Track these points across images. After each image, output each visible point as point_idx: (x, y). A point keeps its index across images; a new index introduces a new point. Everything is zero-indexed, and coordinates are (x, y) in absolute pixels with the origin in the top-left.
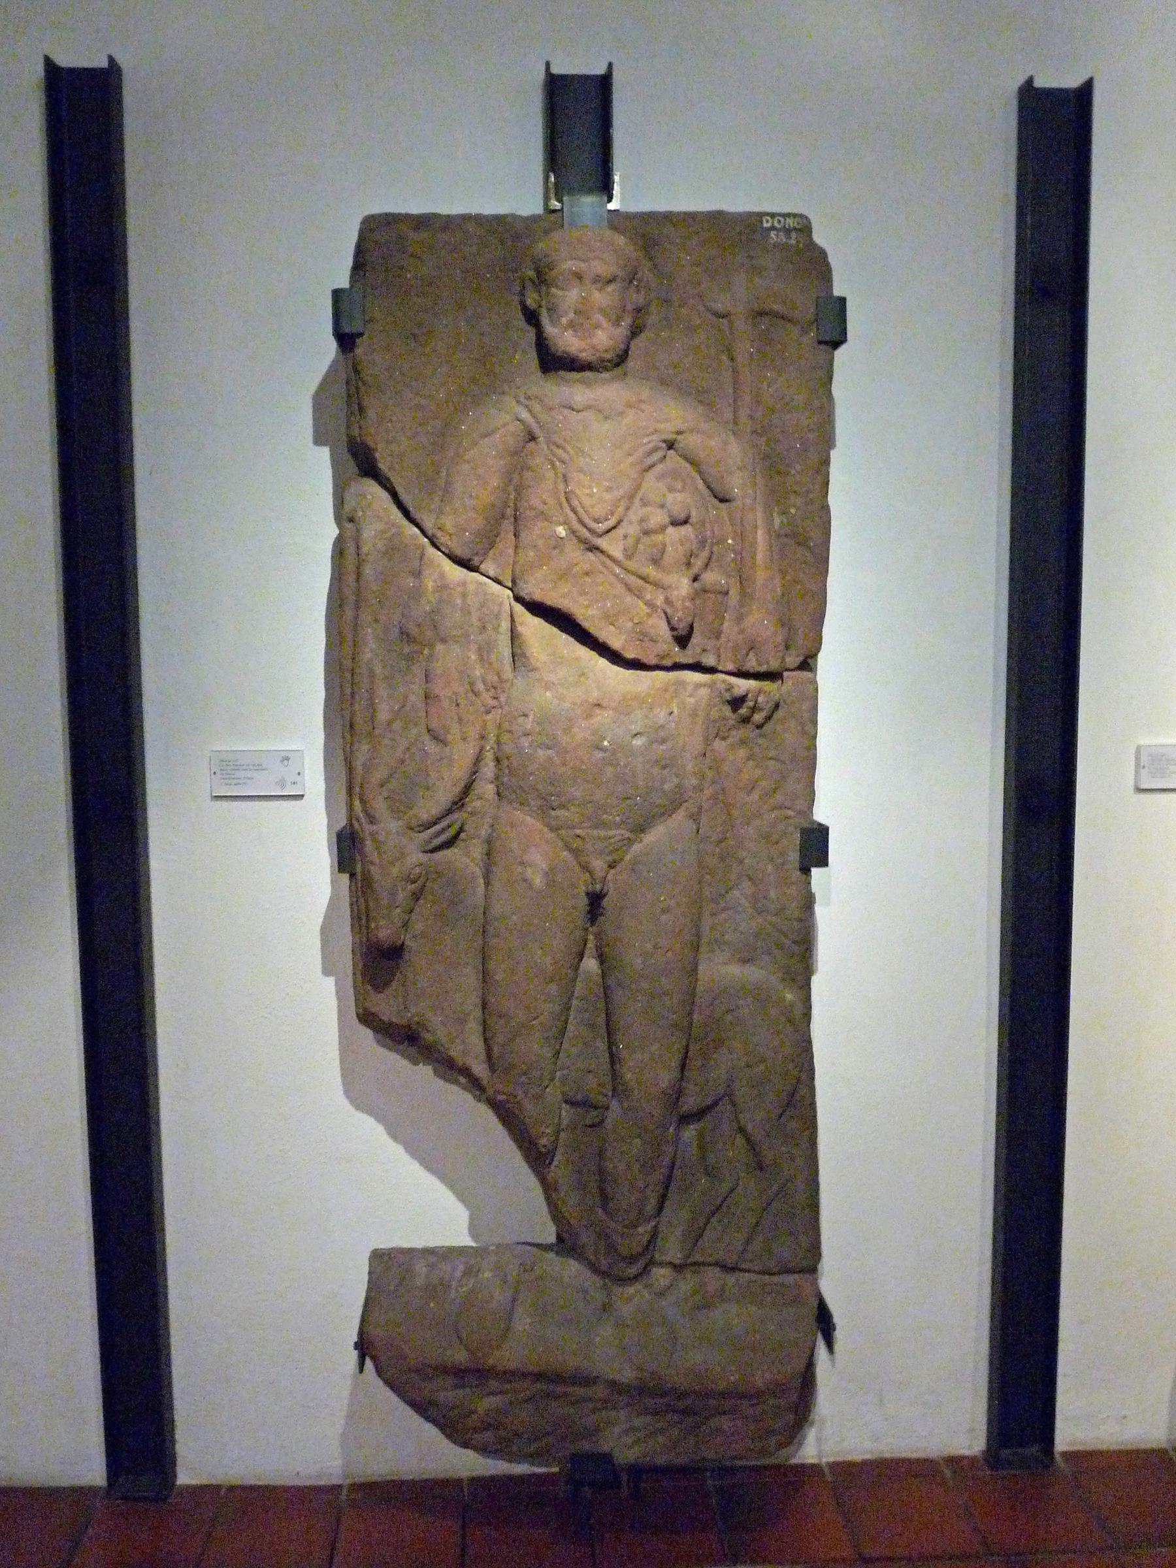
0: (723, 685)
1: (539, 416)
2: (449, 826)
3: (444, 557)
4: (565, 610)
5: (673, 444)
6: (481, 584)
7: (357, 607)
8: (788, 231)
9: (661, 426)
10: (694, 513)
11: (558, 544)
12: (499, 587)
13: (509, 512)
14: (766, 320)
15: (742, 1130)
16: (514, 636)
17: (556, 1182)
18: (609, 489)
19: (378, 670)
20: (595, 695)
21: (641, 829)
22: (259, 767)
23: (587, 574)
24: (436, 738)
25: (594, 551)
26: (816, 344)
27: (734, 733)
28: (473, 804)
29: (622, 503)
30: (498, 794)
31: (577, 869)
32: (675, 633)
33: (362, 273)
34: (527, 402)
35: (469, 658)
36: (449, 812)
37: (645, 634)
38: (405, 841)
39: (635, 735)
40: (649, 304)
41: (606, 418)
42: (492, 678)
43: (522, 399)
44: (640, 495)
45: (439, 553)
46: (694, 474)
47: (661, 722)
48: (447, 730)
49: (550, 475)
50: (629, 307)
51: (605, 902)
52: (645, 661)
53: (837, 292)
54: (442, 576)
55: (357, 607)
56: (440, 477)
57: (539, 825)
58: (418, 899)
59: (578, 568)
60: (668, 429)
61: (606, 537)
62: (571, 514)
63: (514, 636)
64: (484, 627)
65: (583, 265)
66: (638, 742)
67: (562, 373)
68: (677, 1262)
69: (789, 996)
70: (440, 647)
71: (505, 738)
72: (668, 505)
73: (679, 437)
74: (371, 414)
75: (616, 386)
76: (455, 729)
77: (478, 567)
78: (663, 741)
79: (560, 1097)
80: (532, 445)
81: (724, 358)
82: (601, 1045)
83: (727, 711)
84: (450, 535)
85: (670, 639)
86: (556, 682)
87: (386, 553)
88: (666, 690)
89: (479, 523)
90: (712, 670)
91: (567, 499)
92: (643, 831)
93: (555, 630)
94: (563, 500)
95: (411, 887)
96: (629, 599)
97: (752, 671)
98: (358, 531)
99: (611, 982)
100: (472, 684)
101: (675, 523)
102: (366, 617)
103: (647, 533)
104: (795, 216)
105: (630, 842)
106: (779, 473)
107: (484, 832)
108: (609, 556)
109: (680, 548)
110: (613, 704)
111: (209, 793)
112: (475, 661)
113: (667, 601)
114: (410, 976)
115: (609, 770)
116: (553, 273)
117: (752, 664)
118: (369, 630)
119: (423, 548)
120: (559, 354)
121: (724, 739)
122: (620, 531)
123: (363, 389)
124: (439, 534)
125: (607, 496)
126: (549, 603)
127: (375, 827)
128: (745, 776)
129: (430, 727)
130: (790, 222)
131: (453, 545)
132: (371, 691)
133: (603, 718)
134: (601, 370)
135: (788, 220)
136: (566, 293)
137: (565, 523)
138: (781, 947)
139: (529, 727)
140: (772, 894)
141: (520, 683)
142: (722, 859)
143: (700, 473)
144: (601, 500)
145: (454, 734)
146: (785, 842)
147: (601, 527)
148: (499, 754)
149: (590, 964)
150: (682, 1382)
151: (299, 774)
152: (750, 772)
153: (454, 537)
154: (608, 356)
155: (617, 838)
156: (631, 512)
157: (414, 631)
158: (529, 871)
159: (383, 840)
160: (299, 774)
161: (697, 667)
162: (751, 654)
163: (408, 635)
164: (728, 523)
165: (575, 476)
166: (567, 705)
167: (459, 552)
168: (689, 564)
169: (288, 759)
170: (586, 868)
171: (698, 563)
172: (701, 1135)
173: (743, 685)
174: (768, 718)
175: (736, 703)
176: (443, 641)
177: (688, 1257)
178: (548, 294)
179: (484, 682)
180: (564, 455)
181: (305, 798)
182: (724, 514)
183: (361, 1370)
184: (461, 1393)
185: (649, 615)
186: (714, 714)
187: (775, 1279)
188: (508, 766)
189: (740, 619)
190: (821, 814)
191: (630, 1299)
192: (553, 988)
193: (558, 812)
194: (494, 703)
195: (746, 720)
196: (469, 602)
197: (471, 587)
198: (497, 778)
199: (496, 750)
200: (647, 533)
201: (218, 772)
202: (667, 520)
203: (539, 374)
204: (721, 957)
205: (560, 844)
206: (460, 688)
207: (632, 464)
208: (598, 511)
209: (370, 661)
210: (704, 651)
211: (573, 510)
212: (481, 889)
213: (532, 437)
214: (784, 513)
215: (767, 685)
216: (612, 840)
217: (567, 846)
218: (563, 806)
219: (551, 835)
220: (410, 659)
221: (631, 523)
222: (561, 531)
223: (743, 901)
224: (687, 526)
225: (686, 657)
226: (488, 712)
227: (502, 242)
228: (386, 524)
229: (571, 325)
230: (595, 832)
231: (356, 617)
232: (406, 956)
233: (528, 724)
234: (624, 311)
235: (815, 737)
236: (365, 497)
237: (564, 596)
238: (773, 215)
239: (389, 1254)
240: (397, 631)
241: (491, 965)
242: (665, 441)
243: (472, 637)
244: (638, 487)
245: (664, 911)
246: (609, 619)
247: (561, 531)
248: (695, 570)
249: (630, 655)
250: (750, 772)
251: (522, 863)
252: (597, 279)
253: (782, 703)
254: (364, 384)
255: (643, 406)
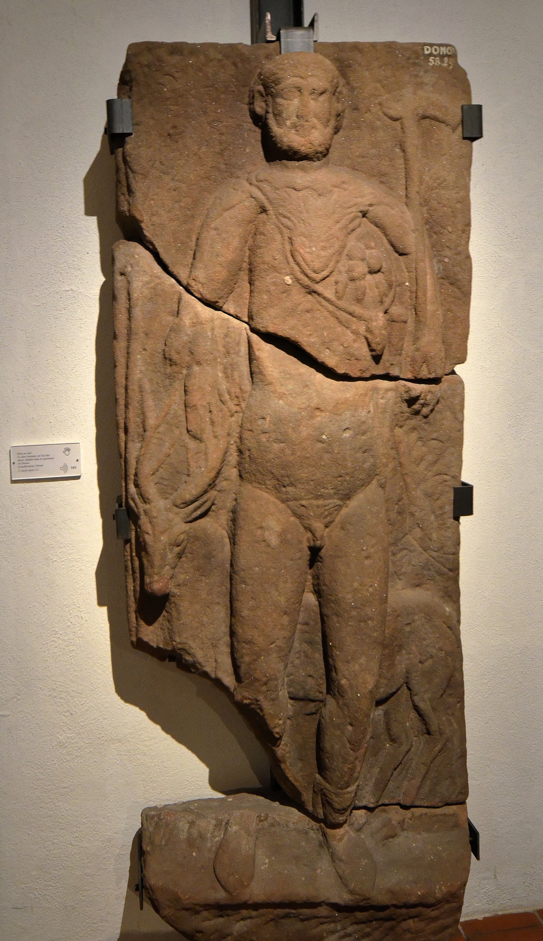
0: (403, 388)
1: (269, 194)
2: (205, 502)
3: (197, 300)
4: (293, 339)
5: (366, 214)
6: (224, 319)
7: (129, 340)
8: (442, 57)
9: (359, 200)
10: (384, 264)
11: (286, 290)
12: (238, 322)
13: (245, 266)
14: (428, 121)
15: (416, 708)
16: (251, 357)
17: (283, 756)
18: (324, 248)
19: (147, 386)
20: (315, 402)
21: (347, 497)
22: (47, 457)
23: (308, 311)
24: (195, 437)
25: (313, 294)
26: (461, 138)
27: (408, 422)
28: (222, 484)
29: (334, 258)
30: (240, 476)
31: (302, 529)
32: (374, 353)
33: (127, 88)
34: (258, 184)
35: (218, 376)
36: (206, 492)
37: (352, 355)
38: (171, 516)
39: (345, 430)
40: (343, 111)
41: (320, 195)
42: (235, 390)
43: (255, 182)
44: (346, 252)
45: (193, 298)
46: (382, 235)
47: (363, 419)
48: (203, 430)
49: (278, 237)
50: (334, 113)
51: (323, 552)
52: (352, 375)
53: (475, 102)
54: (196, 314)
55: (129, 340)
56: (191, 241)
57: (273, 499)
58: (180, 558)
59: (300, 308)
60: (364, 201)
61: (321, 284)
62: (296, 267)
63: (251, 357)
64: (228, 353)
65: (302, 81)
66: (347, 435)
67: (284, 161)
68: (372, 805)
69: (447, 609)
70: (196, 368)
71: (246, 435)
72: (367, 258)
73: (371, 208)
74: (138, 195)
75: (324, 171)
76: (208, 428)
77: (221, 307)
78: (364, 433)
79: (287, 695)
80: (264, 216)
81: (397, 150)
82: (319, 656)
83: (404, 406)
84: (202, 284)
85: (369, 358)
86: (287, 393)
87: (150, 299)
88: (366, 395)
89: (223, 274)
90: (396, 378)
91: (292, 255)
92: (349, 499)
93: (283, 353)
94: (289, 255)
95: (177, 549)
96: (339, 329)
97: (424, 378)
98: (129, 282)
99: (325, 611)
100: (220, 395)
101: (372, 272)
102: (136, 346)
103: (353, 280)
104: (447, 45)
105: (340, 507)
106: (435, 233)
107: (230, 504)
108: (324, 298)
109: (376, 290)
110: (329, 408)
111: (9, 479)
112: (222, 377)
113: (369, 330)
114: (174, 614)
115: (326, 456)
116: (281, 86)
117: (424, 373)
118: (139, 356)
119: (180, 294)
120: (285, 148)
121: (401, 427)
122: (332, 279)
123: (131, 175)
124: (193, 283)
125: (323, 253)
126: (280, 333)
127: (148, 506)
128: (415, 453)
129: (189, 429)
130: (443, 50)
131: (204, 292)
132: (142, 402)
133: (320, 418)
134: (315, 159)
135: (442, 48)
136: (290, 102)
137: (292, 274)
138: (441, 574)
139: (266, 427)
140: (434, 536)
141: (258, 394)
142: (399, 513)
143: (386, 235)
144: (318, 256)
145: (207, 435)
146: (443, 498)
147: (319, 277)
148: (242, 447)
149: (310, 598)
150: (382, 899)
151: (77, 460)
152: (419, 450)
153: (205, 285)
154: (320, 149)
155: (331, 506)
156: (340, 264)
157: (175, 357)
158: (267, 533)
159: (155, 515)
160: (77, 460)
161: (387, 377)
162: (424, 366)
163: (170, 360)
164: (405, 270)
165: (298, 240)
166: (295, 410)
167: (209, 296)
168: (382, 302)
169: (68, 450)
170: (308, 529)
171: (387, 301)
172: (386, 714)
173: (418, 388)
174: (432, 411)
175: (411, 401)
176: (199, 363)
177: (378, 802)
178: (275, 102)
179: (229, 393)
180: (289, 223)
181: (81, 477)
182: (402, 264)
183: (142, 908)
184: (221, 920)
185: (355, 341)
186: (398, 410)
187: (438, 811)
188: (249, 456)
189: (416, 339)
190: (466, 477)
191: (341, 839)
192: (285, 620)
193: (290, 489)
194: (238, 408)
195: (417, 413)
196: (215, 333)
197: (217, 323)
198: (239, 464)
199: (239, 444)
200: (353, 280)
201: (17, 462)
202: (367, 270)
203: (264, 162)
204: (400, 584)
205: (289, 512)
206: (214, 400)
207: (341, 229)
208: (317, 265)
209: (140, 380)
210: (392, 364)
211: (298, 264)
212: (228, 548)
213: (263, 210)
214: (440, 261)
215: (433, 387)
216: (327, 508)
217: (295, 514)
218: (292, 485)
219: (282, 506)
220: (170, 377)
221: (340, 272)
222: (288, 279)
223: (415, 543)
224: (380, 274)
225: (379, 370)
226: (232, 416)
227: (235, 64)
228: (151, 276)
229: (294, 126)
230: (315, 502)
231: (128, 347)
232: (172, 599)
233: (266, 425)
234: (330, 115)
235: (462, 422)
236: (134, 257)
237: (292, 328)
238: (431, 45)
239: (159, 816)
240: (161, 356)
241: (237, 604)
242: (361, 212)
243: (219, 360)
244: (343, 247)
245: (367, 558)
246: (194, 299)
247: (288, 279)
248: (386, 304)
249: (341, 371)
250: (419, 450)
251: (261, 528)
252: (313, 92)
253: (441, 400)
254: (133, 172)
255: (345, 186)
